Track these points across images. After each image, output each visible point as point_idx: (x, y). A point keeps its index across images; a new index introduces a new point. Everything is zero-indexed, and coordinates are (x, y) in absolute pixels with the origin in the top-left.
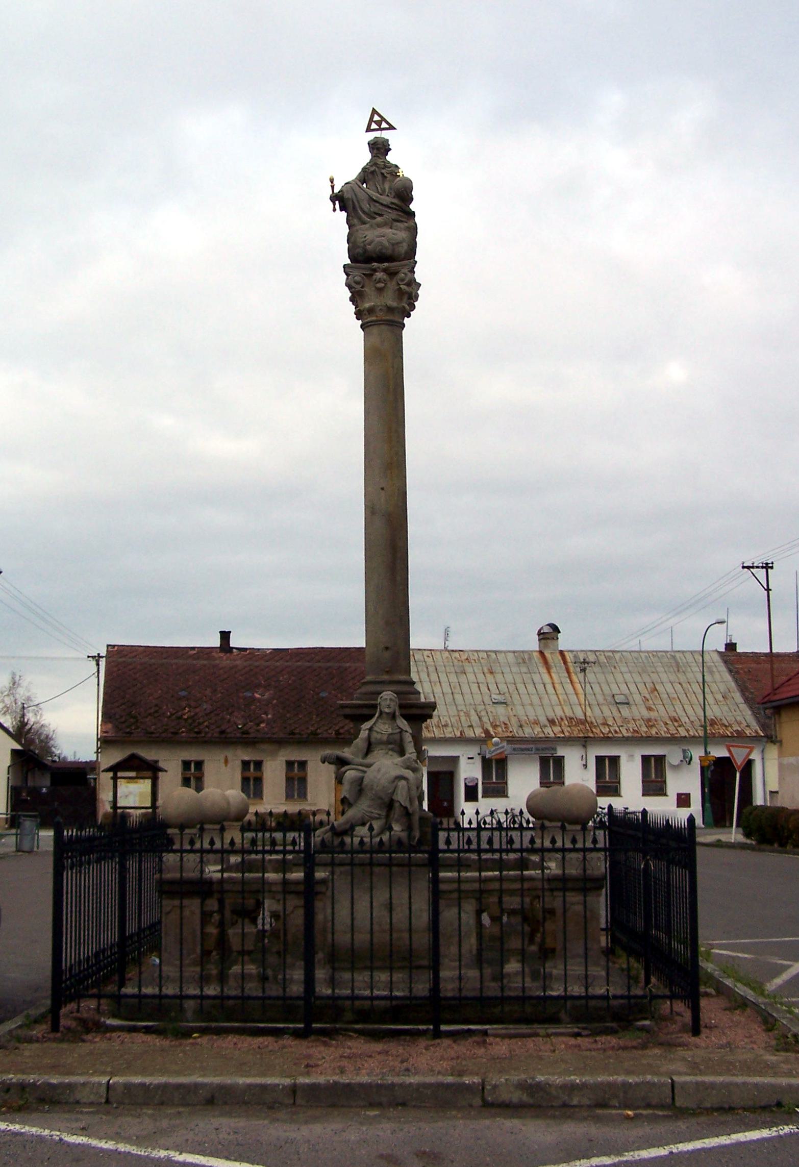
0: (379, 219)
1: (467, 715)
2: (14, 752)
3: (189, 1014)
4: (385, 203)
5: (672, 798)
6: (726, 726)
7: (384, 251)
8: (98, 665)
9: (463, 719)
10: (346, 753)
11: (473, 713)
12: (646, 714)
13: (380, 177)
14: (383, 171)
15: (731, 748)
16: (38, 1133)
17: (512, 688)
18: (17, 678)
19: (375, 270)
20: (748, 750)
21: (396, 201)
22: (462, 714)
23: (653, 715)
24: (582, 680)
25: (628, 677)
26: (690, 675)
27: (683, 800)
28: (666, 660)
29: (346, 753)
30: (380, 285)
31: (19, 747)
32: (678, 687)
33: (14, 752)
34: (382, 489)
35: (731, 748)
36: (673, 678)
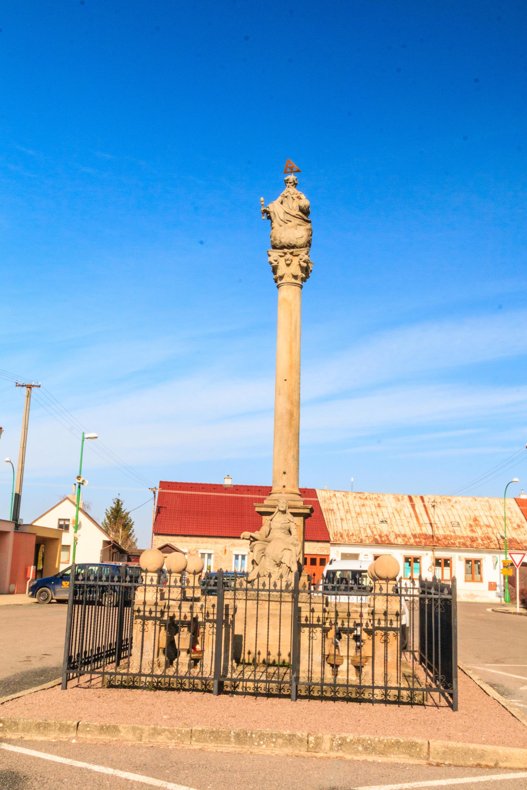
0: (289, 223)
1: (365, 529)
2: (106, 543)
3: (326, 745)
4: (293, 214)
5: (485, 585)
6: (519, 543)
7: (291, 242)
8: (154, 493)
9: (362, 531)
10: (256, 535)
11: (368, 529)
12: (470, 534)
13: (291, 199)
14: (293, 196)
15: (512, 555)
16: (165, 786)
17: (391, 516)
18: (120, 503)
19: (285, 253)
20: (522, 555)
21: (300, 214)
22: (362, 529)
23: (474, 535)
24: (433, 513)
25: (460, 512)
26: (497, 512)
27: (492, 586)
28: (483, 503)
29: (256, 535)
30: (288, 262)
31: (107, 539)
32: (490, 519)
33: (106, 543)
34: (285, 380)
35: (512, 555)
36: (488, 514)
